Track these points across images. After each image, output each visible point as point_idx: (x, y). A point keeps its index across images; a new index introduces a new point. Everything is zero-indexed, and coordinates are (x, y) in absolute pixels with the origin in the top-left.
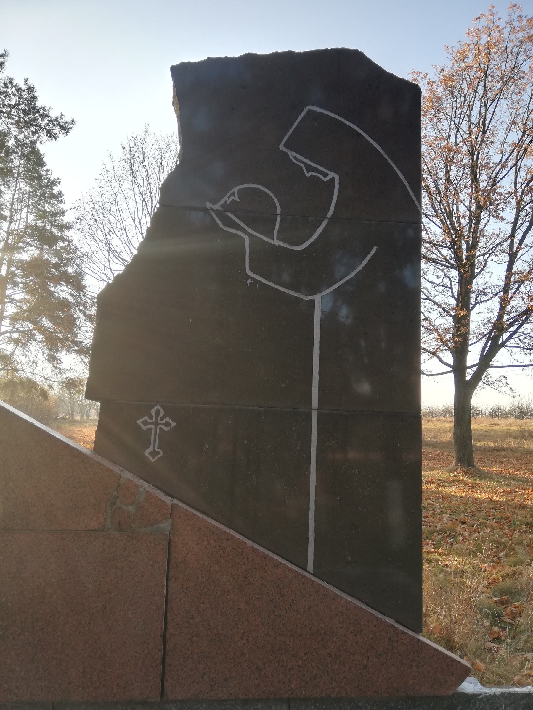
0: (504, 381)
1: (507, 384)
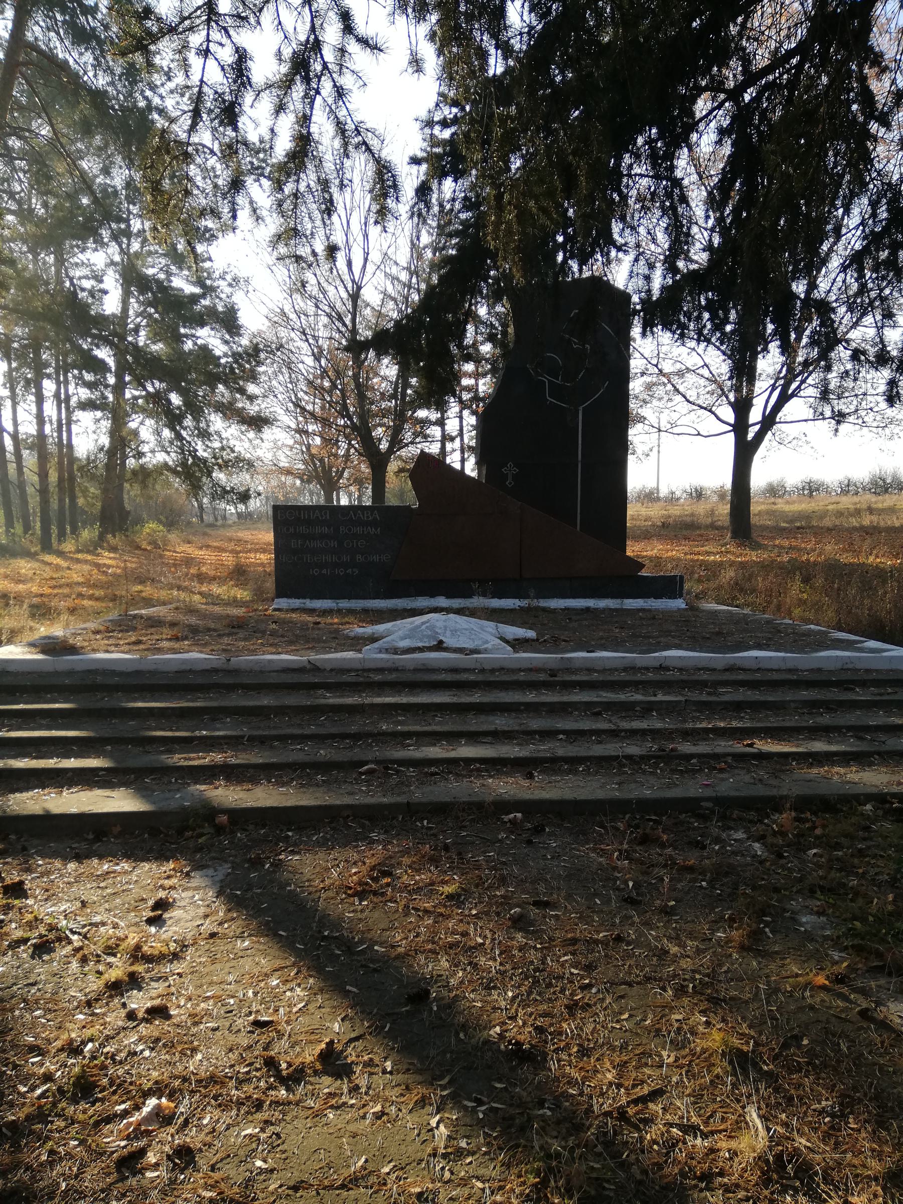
0: (804, 439)
1: (808, 443)
